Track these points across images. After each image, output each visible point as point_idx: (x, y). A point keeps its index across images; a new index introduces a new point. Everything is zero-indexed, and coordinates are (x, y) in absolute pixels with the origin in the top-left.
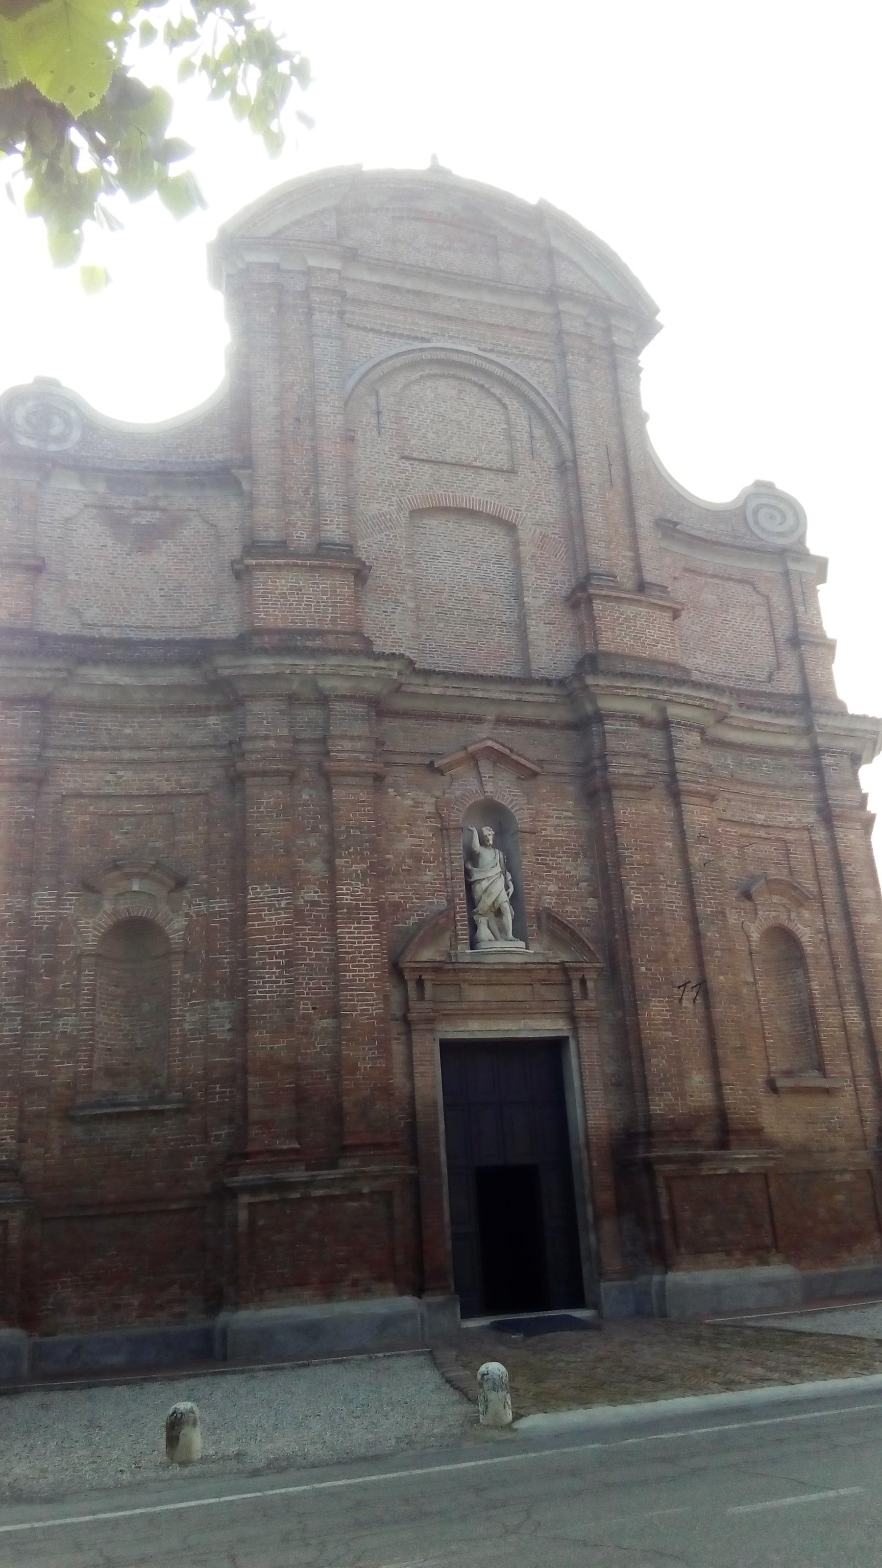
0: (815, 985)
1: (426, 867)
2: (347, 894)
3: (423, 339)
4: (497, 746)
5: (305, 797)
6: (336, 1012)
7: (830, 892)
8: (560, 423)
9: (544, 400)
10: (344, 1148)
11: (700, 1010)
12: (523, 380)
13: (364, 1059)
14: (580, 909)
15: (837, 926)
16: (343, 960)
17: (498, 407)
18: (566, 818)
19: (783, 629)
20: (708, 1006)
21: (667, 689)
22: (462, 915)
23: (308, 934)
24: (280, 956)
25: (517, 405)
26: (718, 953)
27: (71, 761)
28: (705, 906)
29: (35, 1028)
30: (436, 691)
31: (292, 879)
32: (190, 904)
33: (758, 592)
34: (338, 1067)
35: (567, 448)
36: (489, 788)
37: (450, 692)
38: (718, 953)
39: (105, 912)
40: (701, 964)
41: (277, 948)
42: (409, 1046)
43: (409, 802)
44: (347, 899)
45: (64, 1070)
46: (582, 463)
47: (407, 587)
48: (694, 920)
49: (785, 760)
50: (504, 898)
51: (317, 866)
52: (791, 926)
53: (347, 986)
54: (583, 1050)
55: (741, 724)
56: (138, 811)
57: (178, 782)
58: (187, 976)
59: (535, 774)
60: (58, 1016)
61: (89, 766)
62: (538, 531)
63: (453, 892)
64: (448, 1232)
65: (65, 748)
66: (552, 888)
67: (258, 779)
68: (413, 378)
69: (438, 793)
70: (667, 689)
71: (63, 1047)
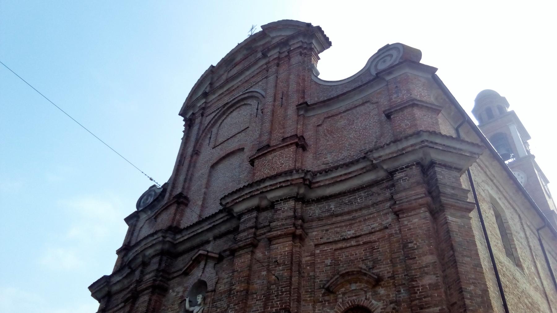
21: (258, 187)
49: (375, 189)
52: (366, 304)
55: (327, 182)
70: (258, 187)
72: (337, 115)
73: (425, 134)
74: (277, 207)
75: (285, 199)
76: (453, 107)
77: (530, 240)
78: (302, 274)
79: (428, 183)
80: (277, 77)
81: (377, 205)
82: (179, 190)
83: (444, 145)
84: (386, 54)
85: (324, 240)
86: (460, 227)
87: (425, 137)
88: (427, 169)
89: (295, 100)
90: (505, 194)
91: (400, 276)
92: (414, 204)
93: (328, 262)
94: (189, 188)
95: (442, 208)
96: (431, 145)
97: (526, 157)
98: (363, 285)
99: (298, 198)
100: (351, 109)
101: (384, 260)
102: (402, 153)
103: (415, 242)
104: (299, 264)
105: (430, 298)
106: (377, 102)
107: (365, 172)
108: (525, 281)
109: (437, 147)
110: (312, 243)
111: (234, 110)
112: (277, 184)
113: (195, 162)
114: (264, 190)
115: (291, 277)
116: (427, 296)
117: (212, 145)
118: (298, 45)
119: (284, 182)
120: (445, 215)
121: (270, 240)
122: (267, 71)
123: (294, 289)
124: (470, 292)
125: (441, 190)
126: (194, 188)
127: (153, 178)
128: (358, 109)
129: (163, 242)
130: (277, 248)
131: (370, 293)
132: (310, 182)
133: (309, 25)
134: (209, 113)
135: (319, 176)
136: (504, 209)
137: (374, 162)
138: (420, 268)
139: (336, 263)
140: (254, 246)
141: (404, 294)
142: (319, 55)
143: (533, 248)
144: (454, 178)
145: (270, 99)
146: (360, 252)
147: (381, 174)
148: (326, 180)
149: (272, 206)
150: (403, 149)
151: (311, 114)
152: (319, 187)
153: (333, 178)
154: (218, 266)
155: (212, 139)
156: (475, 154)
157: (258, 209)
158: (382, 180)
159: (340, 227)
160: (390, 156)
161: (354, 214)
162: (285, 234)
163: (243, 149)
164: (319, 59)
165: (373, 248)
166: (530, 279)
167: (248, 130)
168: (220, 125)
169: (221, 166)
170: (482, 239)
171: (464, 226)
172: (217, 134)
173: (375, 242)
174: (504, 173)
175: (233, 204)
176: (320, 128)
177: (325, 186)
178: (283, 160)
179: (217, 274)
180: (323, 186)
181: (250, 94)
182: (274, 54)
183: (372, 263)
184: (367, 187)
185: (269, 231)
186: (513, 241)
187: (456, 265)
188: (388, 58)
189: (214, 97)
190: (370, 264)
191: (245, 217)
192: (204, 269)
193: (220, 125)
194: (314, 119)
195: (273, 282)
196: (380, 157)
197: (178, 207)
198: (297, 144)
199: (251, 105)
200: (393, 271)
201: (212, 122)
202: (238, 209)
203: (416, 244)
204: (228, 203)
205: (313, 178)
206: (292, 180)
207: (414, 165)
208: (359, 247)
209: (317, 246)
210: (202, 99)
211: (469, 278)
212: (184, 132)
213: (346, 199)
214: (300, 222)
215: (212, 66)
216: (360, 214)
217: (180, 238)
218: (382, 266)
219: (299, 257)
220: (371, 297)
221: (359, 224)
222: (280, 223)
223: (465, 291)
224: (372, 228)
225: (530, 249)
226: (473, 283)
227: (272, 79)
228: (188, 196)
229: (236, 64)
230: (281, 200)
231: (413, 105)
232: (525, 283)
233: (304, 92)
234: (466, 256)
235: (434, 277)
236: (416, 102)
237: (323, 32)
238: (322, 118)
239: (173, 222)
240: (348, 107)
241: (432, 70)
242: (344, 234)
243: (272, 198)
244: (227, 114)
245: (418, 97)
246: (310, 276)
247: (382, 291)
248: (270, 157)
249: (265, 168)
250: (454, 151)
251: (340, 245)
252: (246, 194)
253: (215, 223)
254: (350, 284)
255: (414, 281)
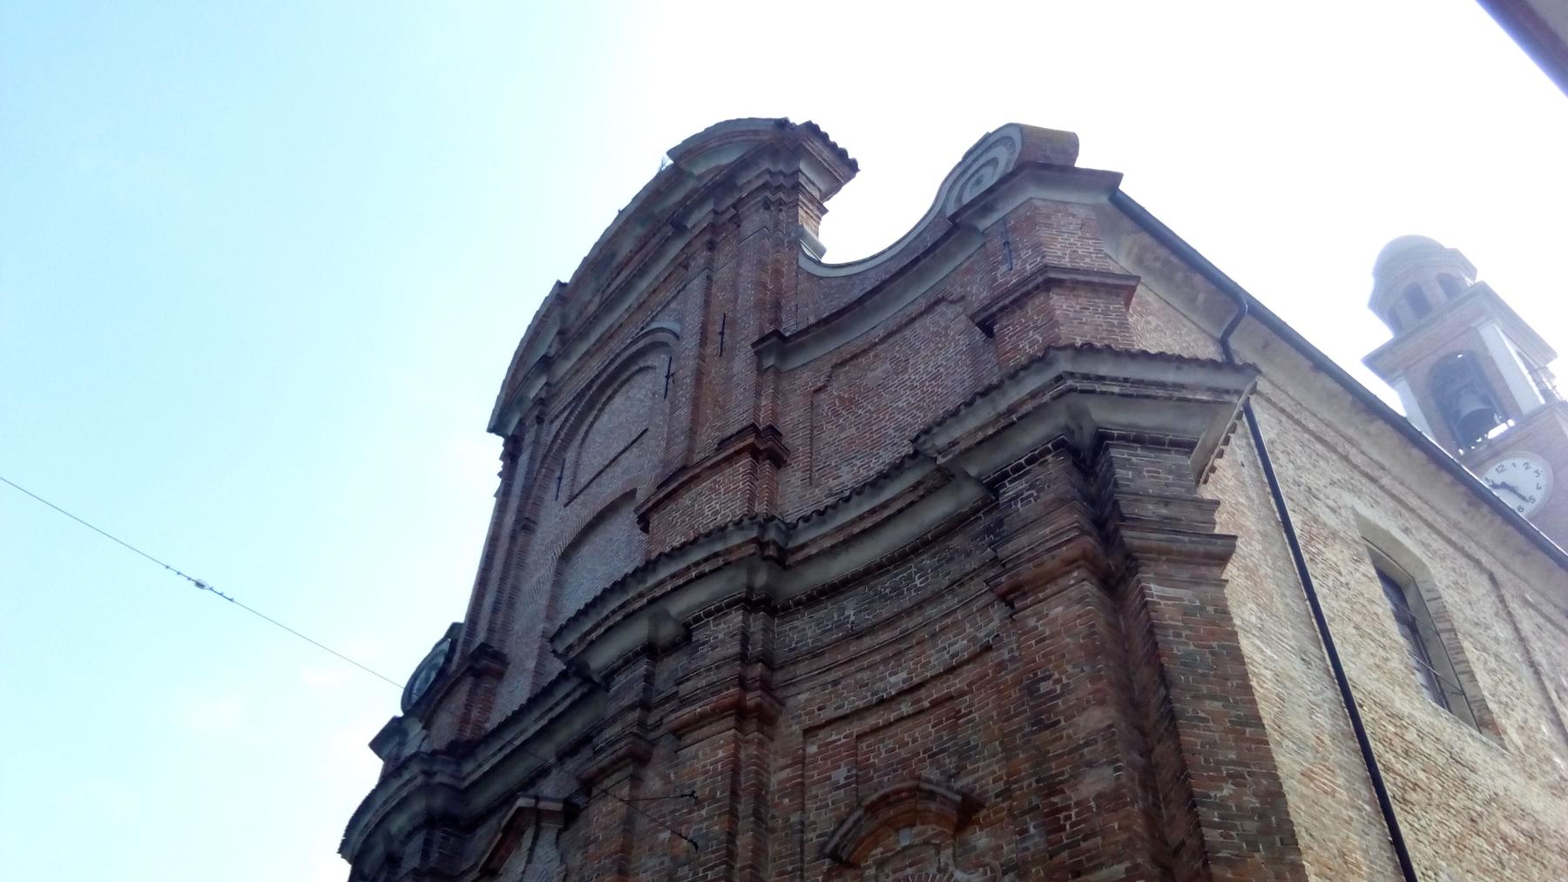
21: (641, 588)
49: (957, 542)
55: (828, 543)
70: (641, 588)
72: (864, 352)
73: (1061, 354)
74: (698, 636)
75: (717, 611)
76: (1198, 279)
77: (1536, 645)
78: (771, 824)
79: (1092, 501)
80: (709, 278)
81: (962, 585)
82: (481, 637)
83: (1126, 380)
84: (982, 161)
85: (830, 713)
86: (1187, 612)
87: (1064, 364)
88: (1088, 456)
89: (750, 328)
90: (1428, 514)
91: (1026, 783)
92: (1050, 563)
93: (840, 775)
94: (506, 627)
95: (1131, 562)
96: (1087, 385)
97: (1539, 411)
98: (930, 830)
99: (750, 603)
100: (900, 329)
101: (984, 745)
102: (1009, 424)
103: (1056, 676)
104: (760, 794)
105: (1099, 840)
106: (963, 298)
107: (922, 497)
108: (1506, 768)
109: (1104, 389)
110: (796, 728)
111: (615, 392)
112: (688, 568)
113: (524, 552)
114: (658, 593)
115: (732, 836)
116: (1093, 834)
117: (563, 498)
118: (760, 182)
119: (706, 560)
120: (1139, 582)
121: (679, 733)
122: (686, 267)
123: (741, 869)
124: (1221, 805)
125: (1125, 511)
126: (518, 626)
127: (203, 580)
128: (917, 324)
129: (428, 789)
130: (696, 757)
131: (949, 851)
132: (780, 549)
133: (782, 124)
134: (556, 412)
135: (805, 529)
136: (1425, 560)
137: (941, 461)
138: (1071, 752)
139: (858, 779)
140: (640, 759)
141: (1037, 839)
142: (826, 204)
143: (1545, 667)
144: (1170, 472)
145: (690, 343)
146: (925, 732)
147: (969, 494)
148: (824, 536)
149: (685, 638)
150: (1011, 410)
151: (797, 361)
152: (808, 559)
153: (840, 529)
154: (566, 836)
155: (564, 482)
156: (1227, 392)
157: (652, 651)
158: (975, 511)
159: (869, 667)
160: (980, 436)
161: (908, 624)
162: (713, 710)
163: (634, 492)
164: (824, 211)
165: (957, 715)
166: (1533, 760)
167: (644, 439)
168: (584, 439)
169: (585, 550)
170: (1312, 649)
171: (1202, 609)
172: (577, 464)
173: (962, 694)
174: (1416, 452)
175: (584, 646)
176: (823, 396)
177: (833, 551)
178: (719, 501)
179: (562, 860)
180: (817, 554)
181: (648, 340)
182: (700, 217)
183: (954, 759)
184: (936, 538)
185: (679, 708)
186: (1461, 650)
187: (1175, 728)
188: (988, 171)
189: (568, 365)
190: (950, 763)
191: (621, 680)
192: (531, 850)
193: (584, 439)
194: (806, 375)
195: (683, 857)
196: (954, 443)
197: (476, 686)
198: (755, 452)
199: (653, 368)
200: (1009, 775)
201: (563, 434)
202: (601, 658)
203: (1059, 681)
204: (570, 648)
205: (788, 537)
206: (728, 551)
207: (1048, 451)
208: (922, 718)
209: (809, 732)
210: (538, 376)
211: (1219, 763)
212: (500, 475)
213: (885, 584)
214: (758, 669)
215: (560, 285)
216: (920, 619)
217: (474, 771)
218: (981, 764)
219: (757, 773)
220: (951, 862)
221: (917, 650)
222: (704, 682)
223: (1203, 804)
224: (953, 656)
225: (1537, 673)
226: (1230, 776)
227: (697, 285)
228: (506, 651)
229: (621, 268)
230: (708, 614)
231: (1049, 285)
232: (1502, 774)
233: (777, 306)
234: (1205, 697)
235: (1108, 772)
236: (1053, 275)
237: (825, 137)
238: (827, 369)
239: (461, 730)
240: (892, 326)
241: (1108, 182)
242: (881, 685)
243: (681, 613)
244: (599, 406)
245: (1066, 262)
246: (791, 826)
247: (981, 839)
248: (686, 500)
249: (673, 529)
250: (1161, 393)
251: (872, 721)
252: (614, 612)
253: (553, 714)
254: (897, 831)
255: (1054, 793)
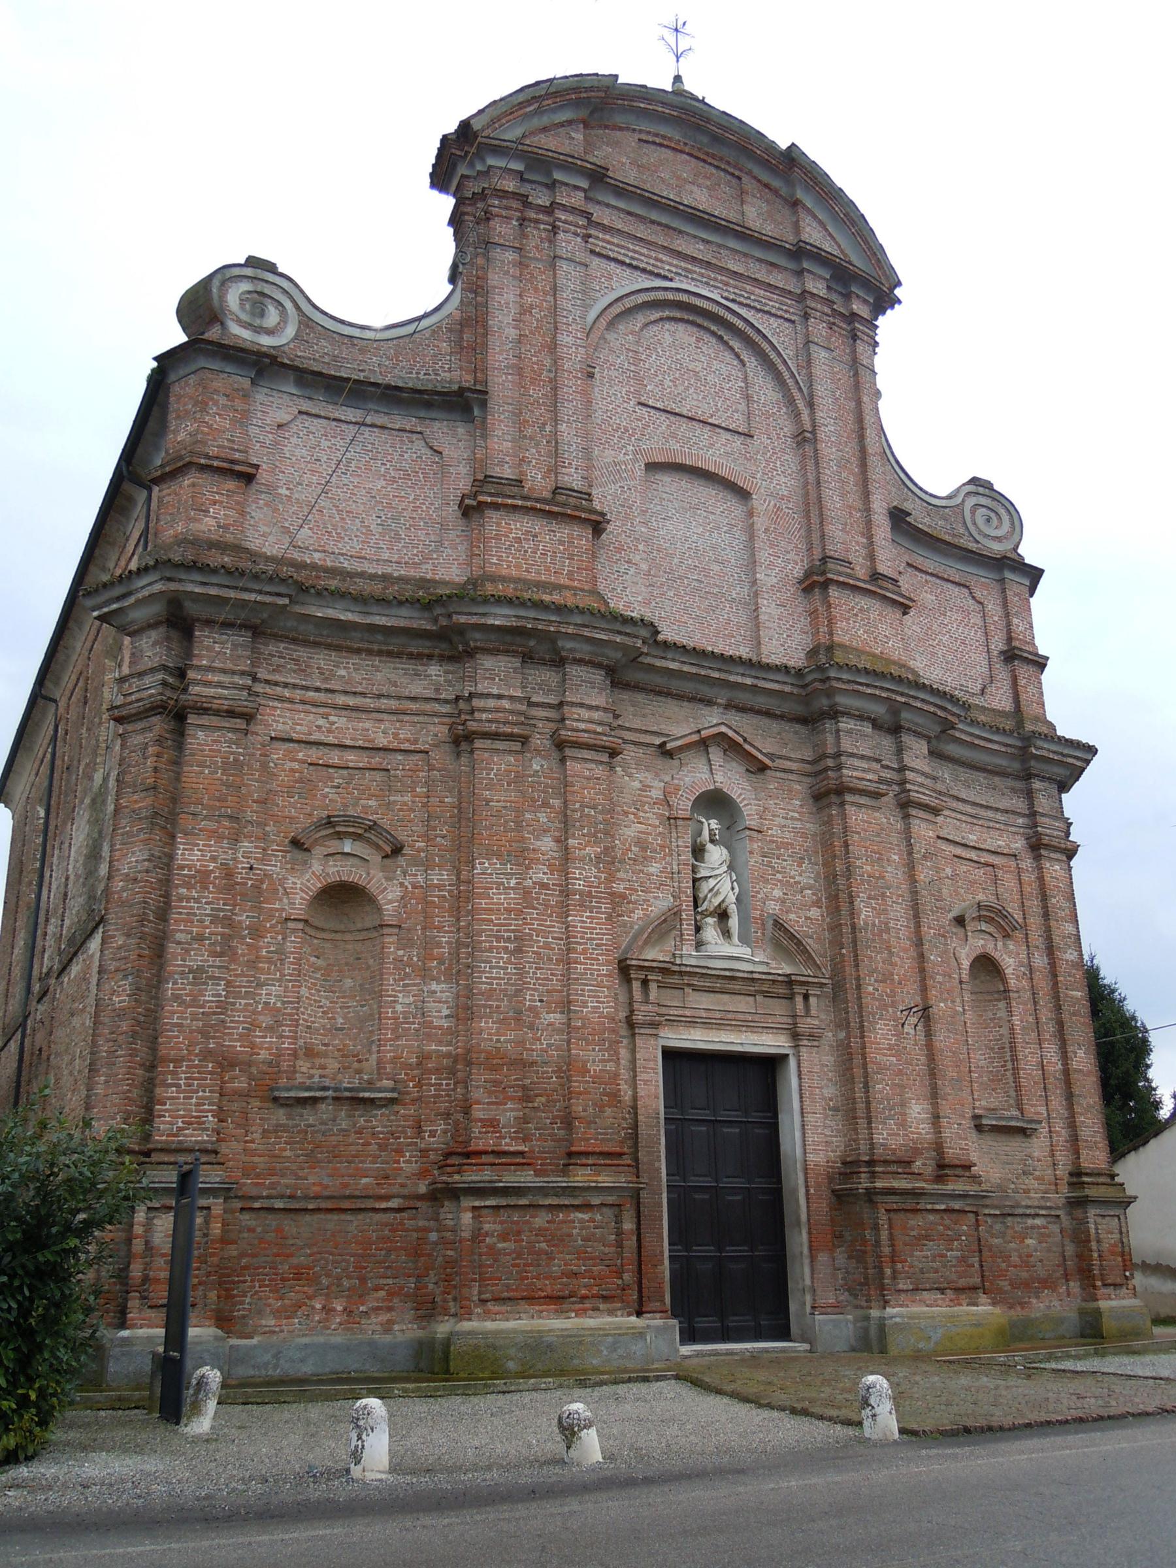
0: (1016, 1020)
1: (652, 857)
2: (579, 879)
3: (665, 278)
4: (730, 733)
5: (536, 767)
6: (566, 1006)
7: (1035, 922)
8: (800, 389)
9: (785, 362)
10: (570, 1154)
11: (921, 1037)
12: (765, 337)
13: (594, 1061)
14: (807, 920)
15: (1040, 960)
16: (575, 951)
17: (735, 363)
18: (792, 818)
19: (998, 643)
20: (929, 1034)
22: (687, 914)
23: (536, 919)
24: (509, 940)
25: (756, 363)
26: (940, 978)
27: (281, 699)
28: (929, 928)
29: (238, 996)
30: (673, 666)
31: (522, 857)
32: (405, 873)
33: (974, 598)
34: (568, 1068)
35: (805, 417)
36: (719, 777)
37: (686, 668)
38: (940, 978)
39: (313, 873)
40: (924, 989)
41: (505, 931)
42: (633, 1051)
43: (637, 784)
44: (579, 885)
45: (266, 1045)
46: (821, 435)
47: (641, 547)
48: (919, 942)
50: (732, 898)
51: (547, 844)
52: (997, 955)
53: (577, 979)
54: (804, 1070)
56: (351, 765)
57: (396, 735)
58: (401, 953)
59: (763, 768)
60: (260, 985)
61: (301, 707)
62: (772, 503)
63: (679, 887)
64: (666, 1254)
65: (276, 684)
66: (777, 893)
67: (487, 743)
68: (652, 318)
69: (667, 778)
71: (265, 1020)
